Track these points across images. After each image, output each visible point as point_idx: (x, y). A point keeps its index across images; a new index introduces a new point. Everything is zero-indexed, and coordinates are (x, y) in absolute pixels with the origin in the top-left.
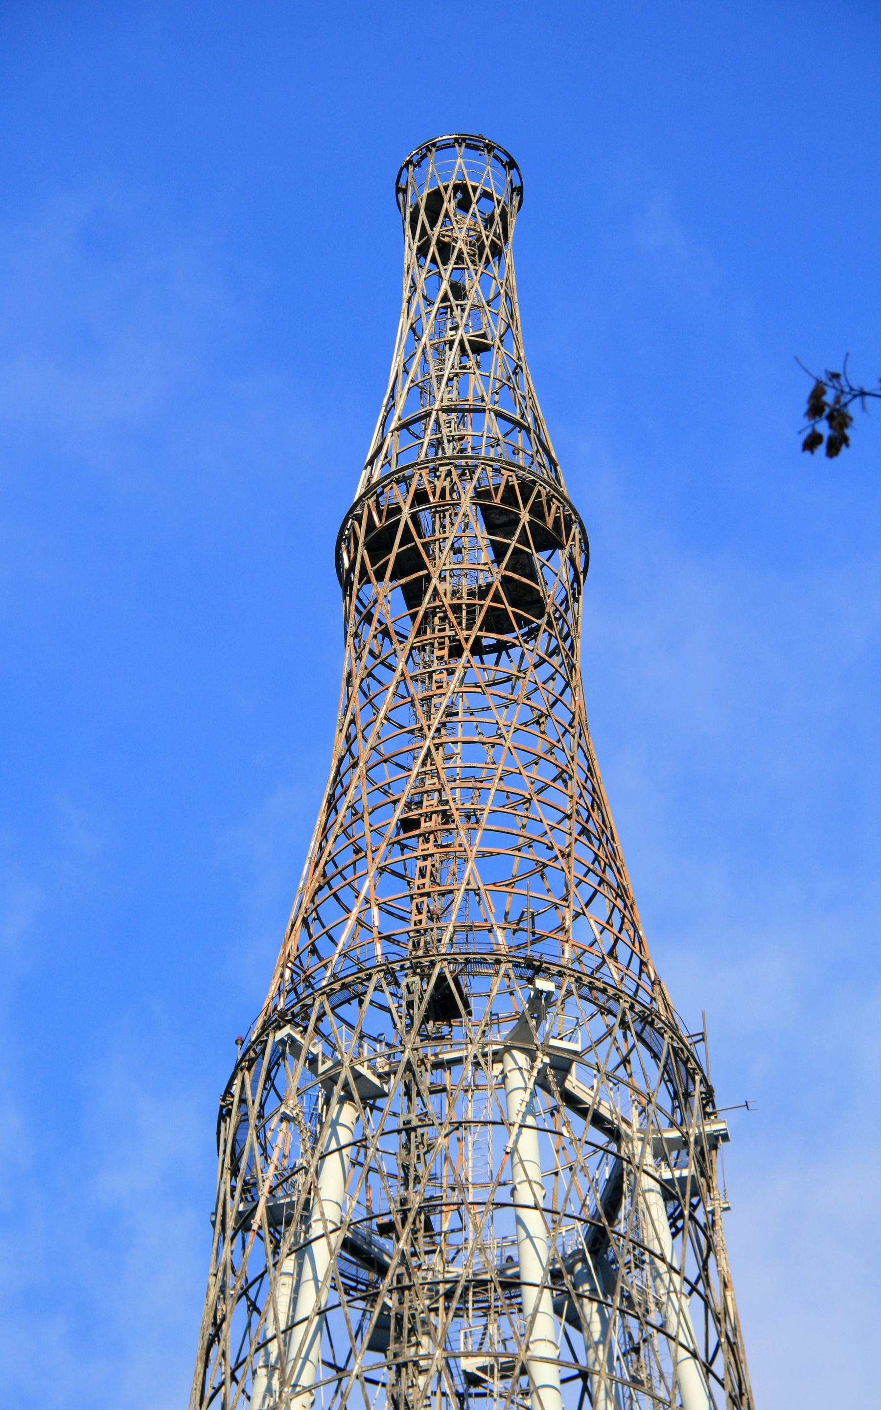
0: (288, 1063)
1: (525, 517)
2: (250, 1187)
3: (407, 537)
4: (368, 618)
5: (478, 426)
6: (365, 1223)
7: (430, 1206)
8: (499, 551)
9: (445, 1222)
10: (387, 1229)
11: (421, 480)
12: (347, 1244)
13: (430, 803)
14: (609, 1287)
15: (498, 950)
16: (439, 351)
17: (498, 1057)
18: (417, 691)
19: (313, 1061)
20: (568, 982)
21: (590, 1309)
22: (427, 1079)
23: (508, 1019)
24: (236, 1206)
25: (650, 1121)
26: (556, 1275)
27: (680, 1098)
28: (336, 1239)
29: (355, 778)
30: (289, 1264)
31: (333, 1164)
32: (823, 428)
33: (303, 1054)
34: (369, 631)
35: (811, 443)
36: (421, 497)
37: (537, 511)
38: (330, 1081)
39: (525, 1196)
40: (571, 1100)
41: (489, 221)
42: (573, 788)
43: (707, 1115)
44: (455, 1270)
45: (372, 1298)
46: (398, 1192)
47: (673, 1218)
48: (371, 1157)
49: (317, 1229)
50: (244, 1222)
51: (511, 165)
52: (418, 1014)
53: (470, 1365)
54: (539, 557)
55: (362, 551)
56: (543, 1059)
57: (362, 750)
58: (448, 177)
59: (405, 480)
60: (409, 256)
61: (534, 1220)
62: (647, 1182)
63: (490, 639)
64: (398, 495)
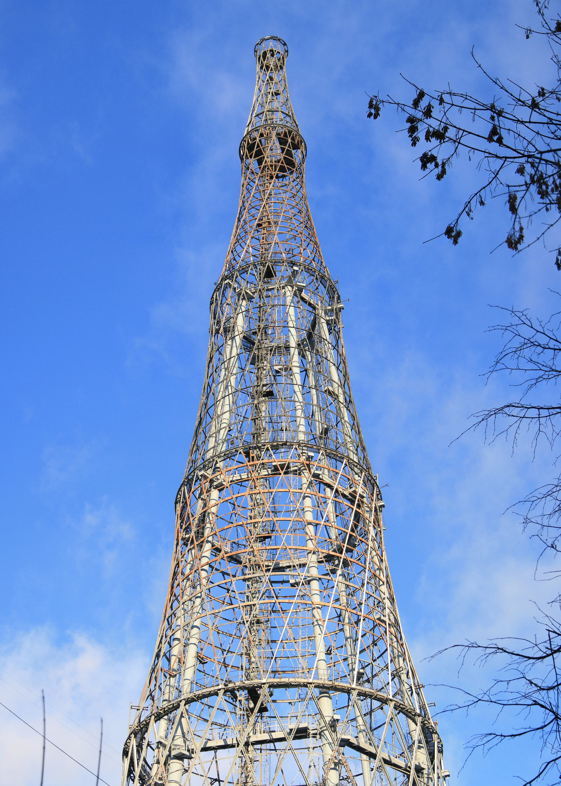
0: (228, 289)
1: (290, 140)
2: (219, 322)
3: (258, 146)
4: (248, 168)
7: (266, 328)
8: (283, 150)
9: (270, 331)
10: (255, 333)
11: (262, 130)
12: (244, 337)
13: (265, 219)
14: (313, 349)
17: (283, 288)
18: (261, 189)
19: (235, 289)
20: (302, 267)
22: (265, 294)
24: (215, 327)
26: (299, 345)
27: (331, 298)
28: (242, 336)
29: (245, 212)
30: (229, 342)
36: (262, 135)
37: (293, 139)
38: (239, 294)
39: (291, 324)
40: (303, 299)
42: (303, 215)
47: (329, 330)
49: (236, 333)
50: (217, 331)
51: (285, 44)
52: (262, 276)
53: (277, 368)
55: (246, 150)
57: (247, 205)
61: (293, 331)
62: (322, 320)
63: (281, 174)
64: (256, 135)
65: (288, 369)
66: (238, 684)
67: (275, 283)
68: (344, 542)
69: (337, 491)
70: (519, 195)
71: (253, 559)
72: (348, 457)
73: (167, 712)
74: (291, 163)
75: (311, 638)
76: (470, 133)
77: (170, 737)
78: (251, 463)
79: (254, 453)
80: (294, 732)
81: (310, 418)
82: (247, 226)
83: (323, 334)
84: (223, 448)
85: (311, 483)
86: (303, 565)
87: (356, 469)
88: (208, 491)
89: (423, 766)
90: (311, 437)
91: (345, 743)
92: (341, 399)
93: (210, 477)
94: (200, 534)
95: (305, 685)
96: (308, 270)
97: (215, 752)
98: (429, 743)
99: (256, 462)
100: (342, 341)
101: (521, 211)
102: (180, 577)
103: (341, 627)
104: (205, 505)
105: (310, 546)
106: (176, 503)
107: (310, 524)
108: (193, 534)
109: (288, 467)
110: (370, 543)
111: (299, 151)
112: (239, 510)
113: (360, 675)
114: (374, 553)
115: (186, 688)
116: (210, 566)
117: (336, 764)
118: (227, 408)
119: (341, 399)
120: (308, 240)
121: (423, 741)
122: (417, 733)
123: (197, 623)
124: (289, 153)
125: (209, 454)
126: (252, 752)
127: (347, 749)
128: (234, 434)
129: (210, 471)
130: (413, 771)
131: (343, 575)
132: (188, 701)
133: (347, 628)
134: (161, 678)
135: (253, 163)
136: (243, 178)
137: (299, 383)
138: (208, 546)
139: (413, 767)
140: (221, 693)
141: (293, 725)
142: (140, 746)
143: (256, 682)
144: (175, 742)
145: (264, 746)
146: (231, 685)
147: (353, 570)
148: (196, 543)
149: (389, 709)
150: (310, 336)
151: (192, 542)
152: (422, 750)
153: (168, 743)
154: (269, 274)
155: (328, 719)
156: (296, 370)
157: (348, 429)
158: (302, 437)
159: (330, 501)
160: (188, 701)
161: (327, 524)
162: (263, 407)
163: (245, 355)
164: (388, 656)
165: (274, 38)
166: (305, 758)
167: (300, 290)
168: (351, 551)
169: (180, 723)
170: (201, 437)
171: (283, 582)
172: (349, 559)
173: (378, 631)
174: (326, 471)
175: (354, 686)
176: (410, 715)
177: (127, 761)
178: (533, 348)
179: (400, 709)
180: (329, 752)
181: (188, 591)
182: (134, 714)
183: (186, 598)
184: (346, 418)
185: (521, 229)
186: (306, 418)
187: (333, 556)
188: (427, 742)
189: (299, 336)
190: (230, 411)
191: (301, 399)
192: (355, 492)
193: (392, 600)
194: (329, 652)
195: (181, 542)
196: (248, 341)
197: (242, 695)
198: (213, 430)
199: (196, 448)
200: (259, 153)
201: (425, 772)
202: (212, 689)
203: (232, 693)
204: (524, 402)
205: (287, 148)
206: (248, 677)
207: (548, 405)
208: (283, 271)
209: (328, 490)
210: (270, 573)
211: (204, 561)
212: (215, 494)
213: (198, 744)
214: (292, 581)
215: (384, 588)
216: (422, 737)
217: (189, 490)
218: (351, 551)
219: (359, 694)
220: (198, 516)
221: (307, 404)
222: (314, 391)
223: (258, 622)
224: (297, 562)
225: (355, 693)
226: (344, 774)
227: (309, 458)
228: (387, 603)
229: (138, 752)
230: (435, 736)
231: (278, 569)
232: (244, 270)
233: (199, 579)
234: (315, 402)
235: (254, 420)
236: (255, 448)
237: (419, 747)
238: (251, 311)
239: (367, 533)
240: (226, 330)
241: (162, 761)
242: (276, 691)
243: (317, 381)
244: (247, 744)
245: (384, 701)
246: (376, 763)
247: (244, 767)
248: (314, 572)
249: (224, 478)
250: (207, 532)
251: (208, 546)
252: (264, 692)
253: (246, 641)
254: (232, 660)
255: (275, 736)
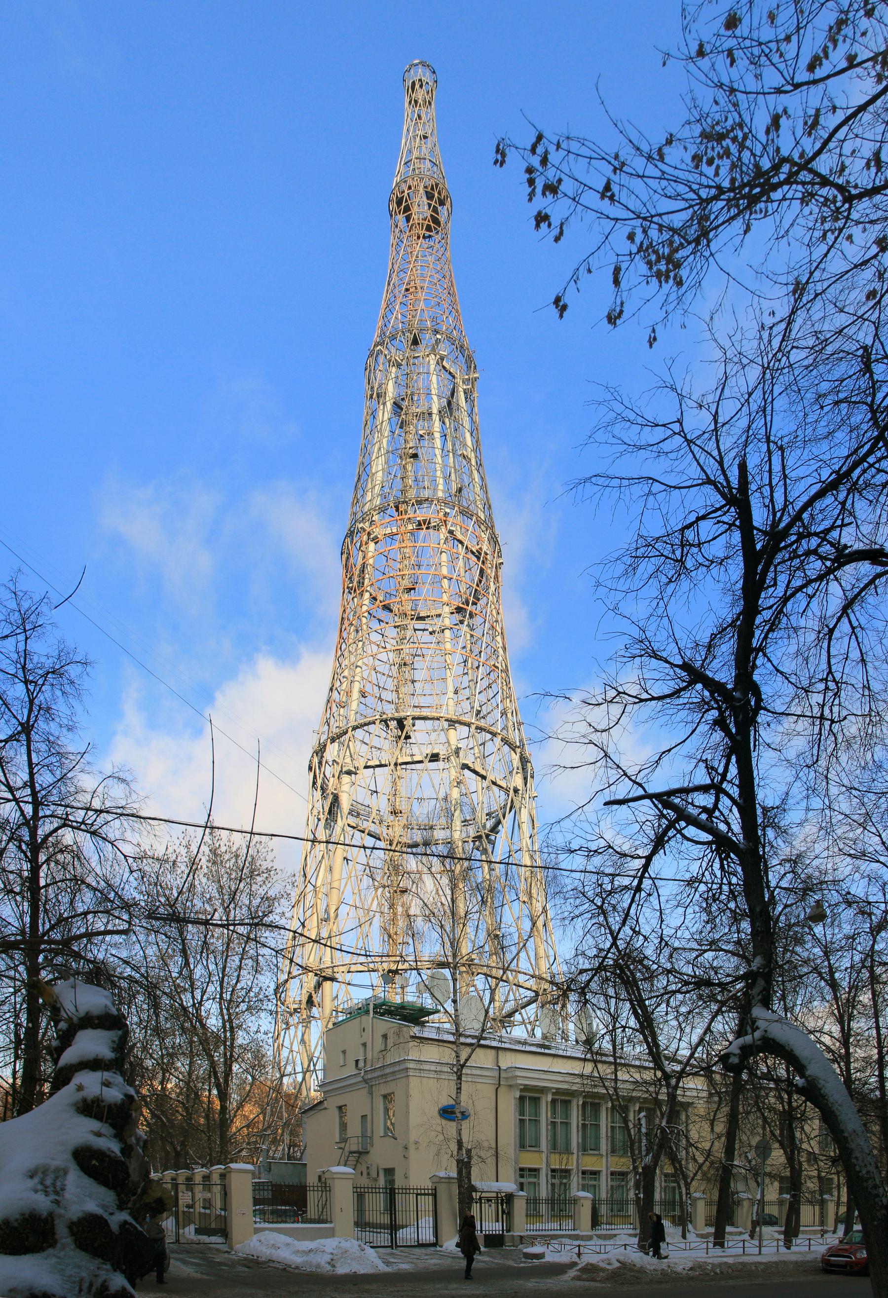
0: (380, 356)
1: (436, 195)
2: (372, 388)
3: (406, 201)
4: (397, 226)
5: (424, 164)
6: (577, 875)
7: (412, 394)
8: (430, 205)
9: (415, 398)
10: (403, 399)
11: (410, 182)
12: (394, 403)
13: (412, 283)
14: (451, 415)
15: (342, 817)
16: (414, 138)
17: (428, 356)
18: (409, 250)
19: (386, 356)
20: (444, 336)
21: (447, 420)
22: (412, 361)
23: (478, 1072)
24: (369, 393)
25: (698, 109)
26: (440, 412)
27: (469, 367)
28: (392, 401)
29: (394, 276)
30: (382, 407)
31: (391, 382)
32: (499, 157)
33: (61, 1230)
34: (397, 230)
35: (496, 162)
36: (410, 188)
37: (439, 193)
38: (390, 361)
39: (433, 392)
40: (444, 367)
41: (428, 93)
42: (447, 281)
43: (96, 1276)
44: (418, 410)
45: (400, 416)
46: (405, 390)
47: (466, 398)
48: (399, 381)
49: (387, 399)
50: (371, 397)
51: (434, 72)
52: (410, 343)
53: (421, 432)
54: (439, 208)
55: (395, 205)
56: (438, 357)
57: (396, 267)
58: (416, 76)
59: (405, 182)
60: (407, 105)
61: (435, 398)
62: (460, 389)
63: (428, 233)
64: (404, 187)
65: (430, 434)
66: (390, 716)
67: (421, 350)
68: (470, 595)
69: (467, 548)
70: (624, 266)
71: (401, 608)
72: (477, 514)
73: (339, 736)
74: (436, 221)
75: (444, 679)
76: (591, 188)
77: (342, 756)
78: (400, 517)
79: (402, 508)
80: (429, 756)
81: (447, 478)
82: (397, 291)
83: (460, 402)
84: (378, 501)
85: (447, 539)
86: (439, 616)
87: (482, 527)
88: (367, 543)
89: (519, 788)
90: (447, 495)
91: (465, 766)
92: (473, 462)
93: (368, 530)
94: (361, 583)
95: (438, 719)
96: (449, 338)
97: (473, 1051)
98: (524, 769)
99: (404, 516)
100: (476, 409)
101: (624, 285)
102: (346, 622)
103: (466, 671)
104: (364, 557)
105: (445, 598)
106: (342, 554)
107: (445, 578)
108: (355, 583)
109: (429, 523)
110: (490, 597)
111: (445, 207)
112: (391, 562)
113: (479, 712)
114: (493, 607)
115: (352, 717)
116: (369, 613)
117: (458, 783)
118: (380, 467)
119: (473, 462)
120: (450, 308)
121: (520, 768)
122: (516, 758)
123: (359, 664)
124: (435, 210)
125: (366, 509)
126: (400, 771)
127: (466, 771)
128: (387, 490)
129: (367, 524)
130: (512, 792)
131: (468, 625)
132: (355, 728)
133: (470, 671)
134: (334, 709)
135: (401, 218)
136: (392, 237)
137: (439, 447)
138: (367, 595)
139: (512, 788)
140: (378, 722)
141: (429, 751)
142: (320, 763)
143: (402, 714)
144: (346, 761)
145: (408, 766)
146: (384, 717)
147: (478, 620)
148: (358, 592)
149: (498, 740)
150: (449, 403)
151: (355, 591)
152: (519, 775)
153: (340, 761)
154: (415, 342)
155: (454, 747)
156: (437, 435)
157: (477, 489)
158: (440, 494)
159: (461, 557)
160: (355, 728)
161: (458, 578)
162: (409, 467)
163: (395, 419)
164: (499, 698)
165: (423, 64)
166: (437, 777)
167: (442, 359)
168: (476, 604)
169: (348, 746)
170: (360, 492)
171: (424, 630)
172: (474, 611)
173: (493, 676)
174: (458, 528)
175: (473, 721)
176: (513, 747)
177: (312, 774)
178: (623, 423)
179: (505, 741)
180: (453, 773)
181: (352, 636)
182: (316, 737)
183: (351, 641)
184: (477, 480)
185: (622, 304)
186: (444, 478)
187: (462, 608)
188: (523, 769)
189: (439, 403)
190: (383, 469)
191: (440, 462)
192: (481, 549)
193: (504, 649)
194: (456, 692)
195: (347, 591)
196: (397, 406)
197: (393, 724)
198: (369, 486)
199: (356, 501)
200: (407, 209)
201: (520, 792)
202: (371, 719)
203: (385, 722)
204: (610, 473)
205: (433, 203)
206: (397, 711)
207: (629, 476)
208: (427, 338)
209: (460, 546)
210: (414, 621)
211: (365, 608)
212: (372, 545)
213: (361, 763)
214: (431, 630)
215: (499, 638)
216: (520, 764)
217: (352, 542)
218: (476, 604)
219: (477, 728)
220: (359, 567)
221: (445, 466)
222: (451, 454)
223: (405, 664)
224: (433, 613)
225: (473, 727)
226: (464, 791)
227: (446, 514)
228: (500, 650)
229: (319, 768)
230: (529, 764)
231: (420, 618)
232: (393, 338)
233: (361, 626)
234: (452, 464)
235: (402, 478)
236: (403, 502)
237: (517, 773)
238: (400, 377)
239: (488, 588)
240: (379, 396)
241: (337, 775)
242: (417, 722)
243: (454, 445)
244: (396, 764)
245: (494, 734)
246: (486, 784)
247: (394, 782)
248: (447, 622)
249: (378, 532)
250: (366, 582)
251: (367, 595)
252: (408, 723)
253: (395, 680)
254: (387, 696)
255: (416, 759)
